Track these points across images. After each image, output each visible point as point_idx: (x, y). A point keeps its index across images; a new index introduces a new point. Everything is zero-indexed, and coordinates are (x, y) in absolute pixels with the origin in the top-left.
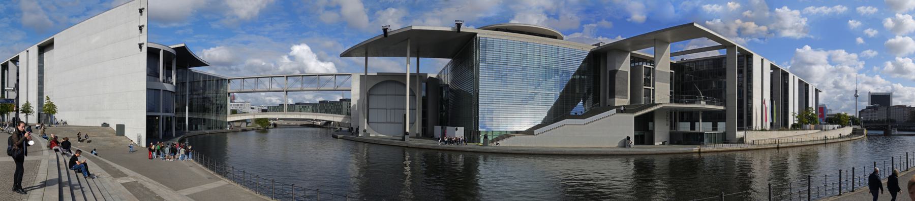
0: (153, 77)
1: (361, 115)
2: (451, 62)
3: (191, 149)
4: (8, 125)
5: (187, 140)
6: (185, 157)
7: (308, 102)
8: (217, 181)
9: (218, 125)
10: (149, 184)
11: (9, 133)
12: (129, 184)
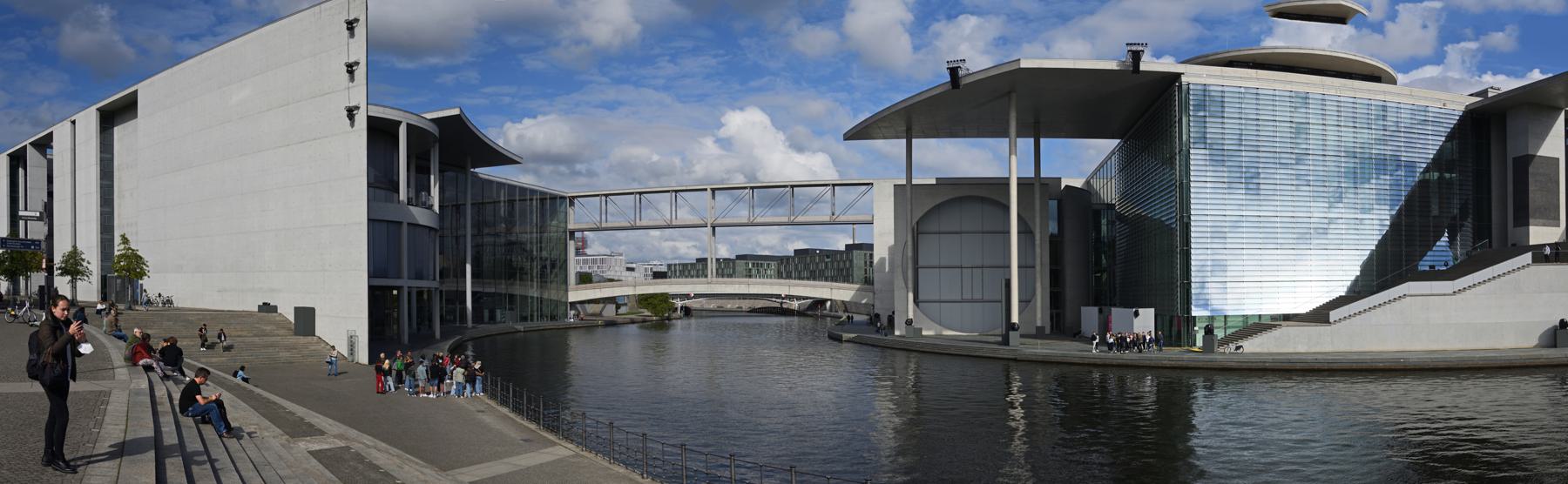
2: (1120, 148)
3: (481, 369)
4: (28, 304)
5: (470, 347)
6: (465, 388)
8: (546, 447)
9: (547, 311)
10: (378, 455)
11: (28, 322)
12: (329, 454)
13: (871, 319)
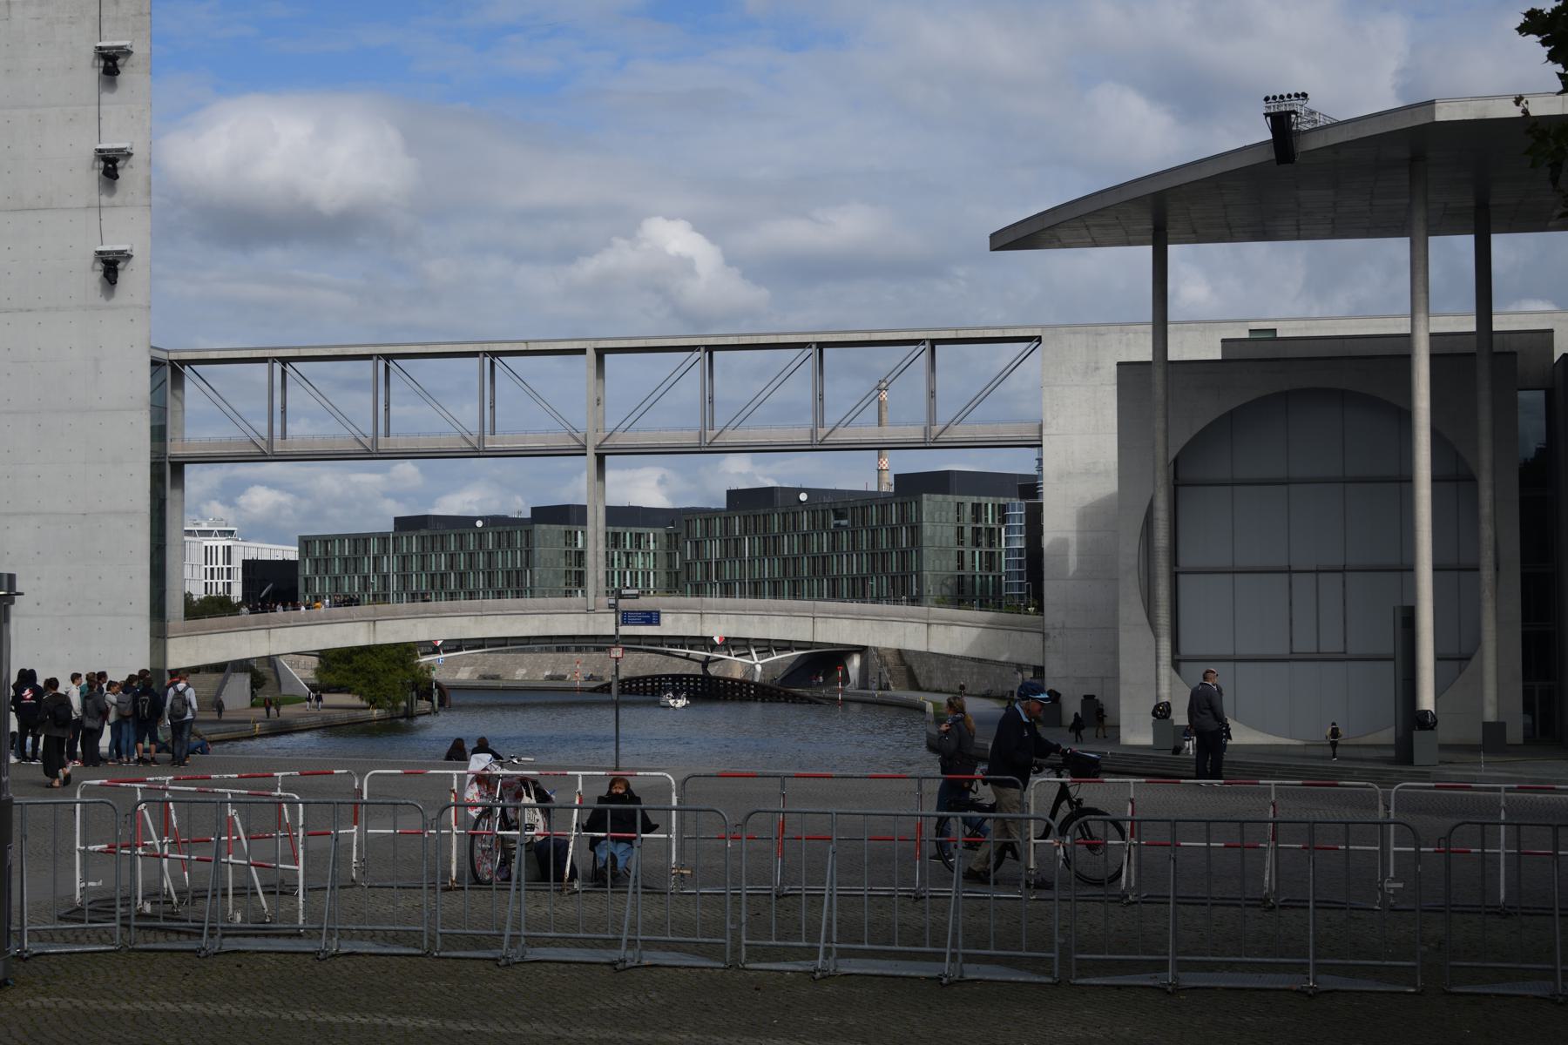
1: (1131, 611)
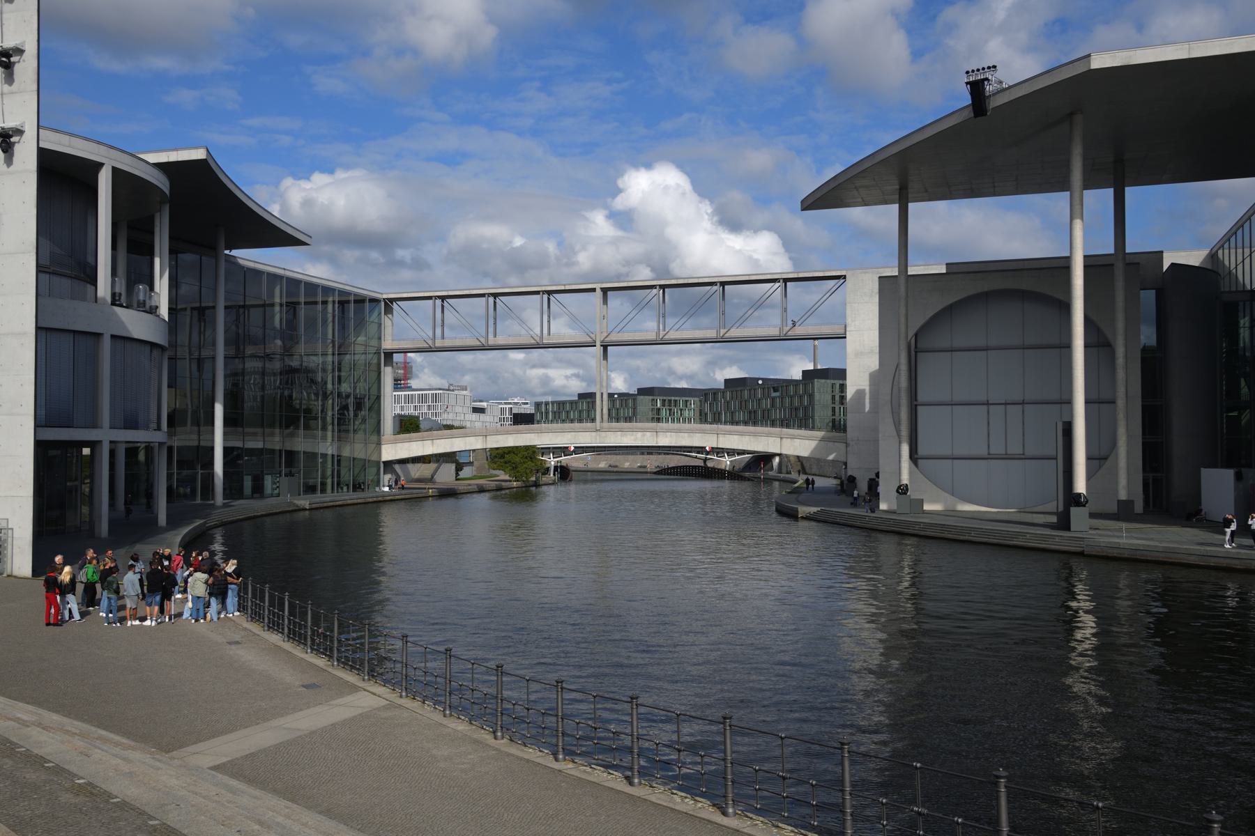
0: (66, 282)
1: (886, 428)
3: (237, 573)
5: (219, 538)
6: (208, 605)
7: (683, 385)
9: (347, 476)
13: (842, 484)
